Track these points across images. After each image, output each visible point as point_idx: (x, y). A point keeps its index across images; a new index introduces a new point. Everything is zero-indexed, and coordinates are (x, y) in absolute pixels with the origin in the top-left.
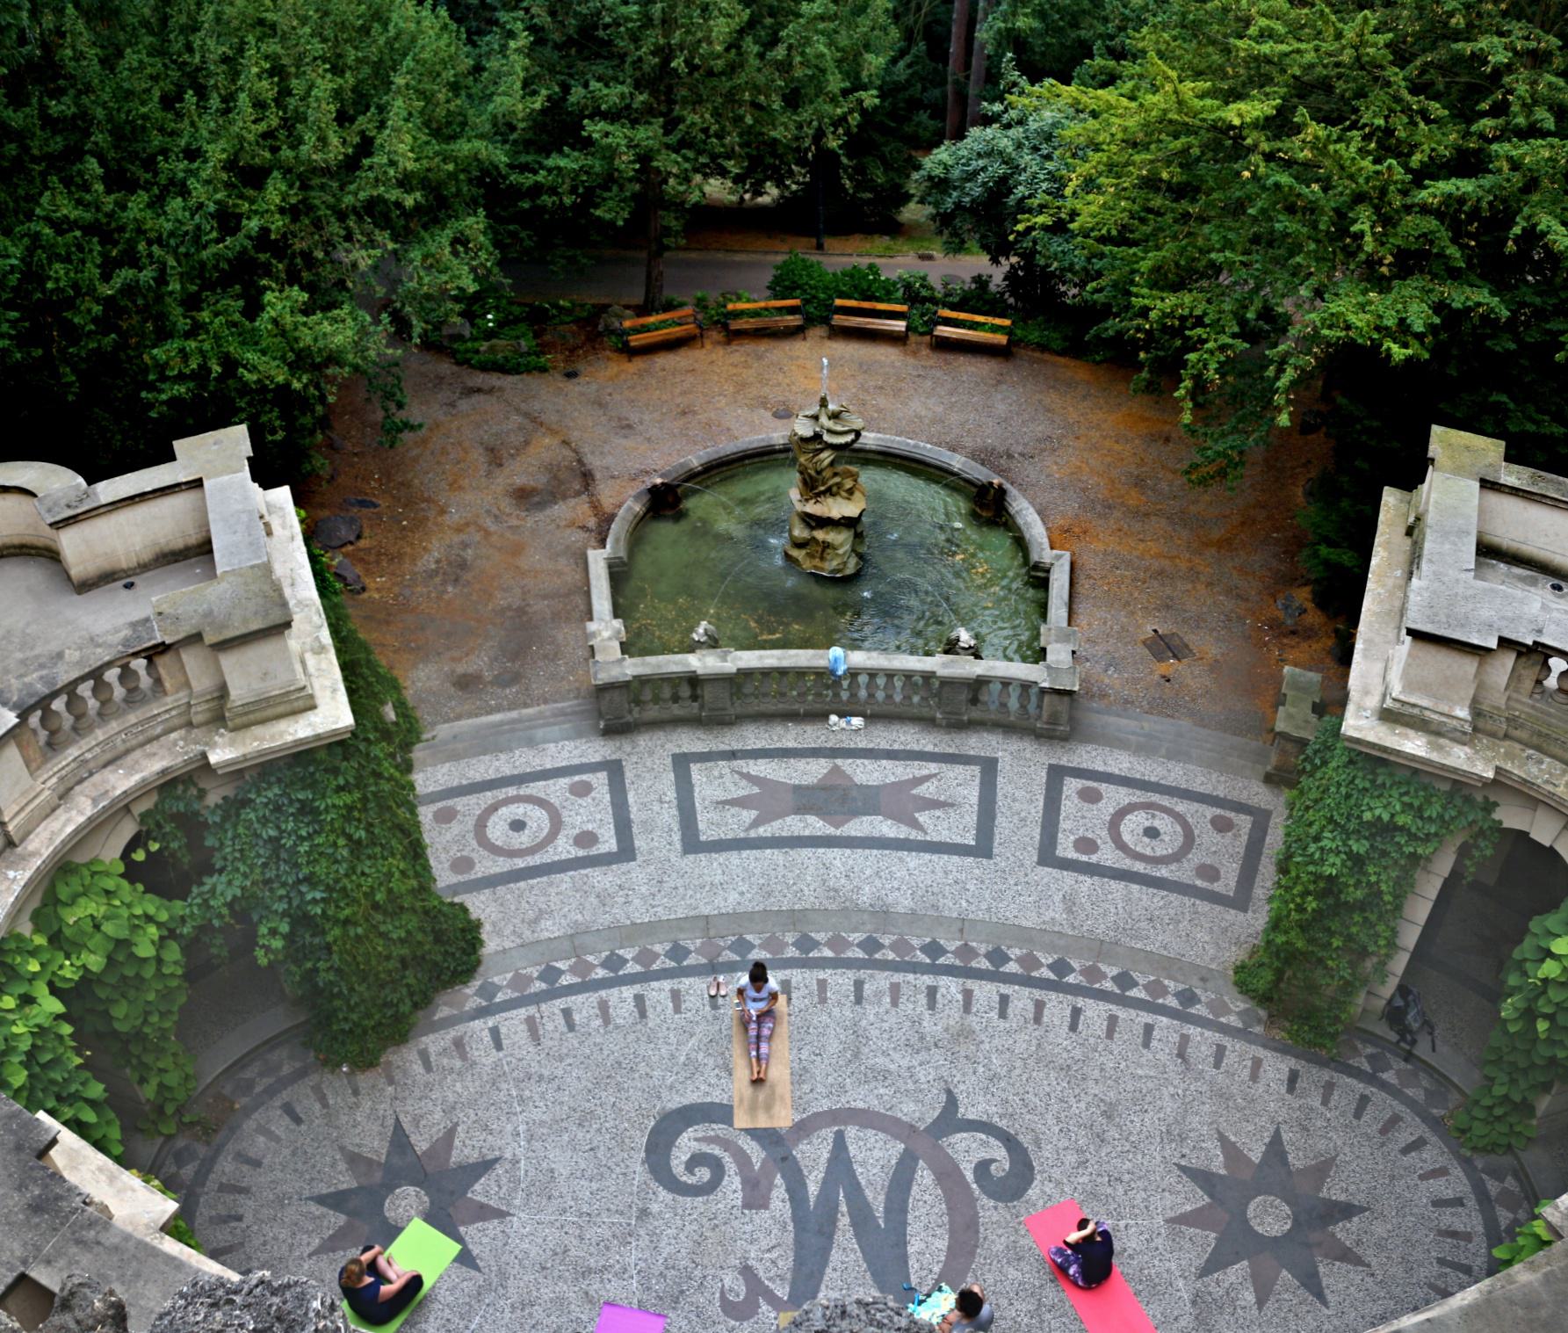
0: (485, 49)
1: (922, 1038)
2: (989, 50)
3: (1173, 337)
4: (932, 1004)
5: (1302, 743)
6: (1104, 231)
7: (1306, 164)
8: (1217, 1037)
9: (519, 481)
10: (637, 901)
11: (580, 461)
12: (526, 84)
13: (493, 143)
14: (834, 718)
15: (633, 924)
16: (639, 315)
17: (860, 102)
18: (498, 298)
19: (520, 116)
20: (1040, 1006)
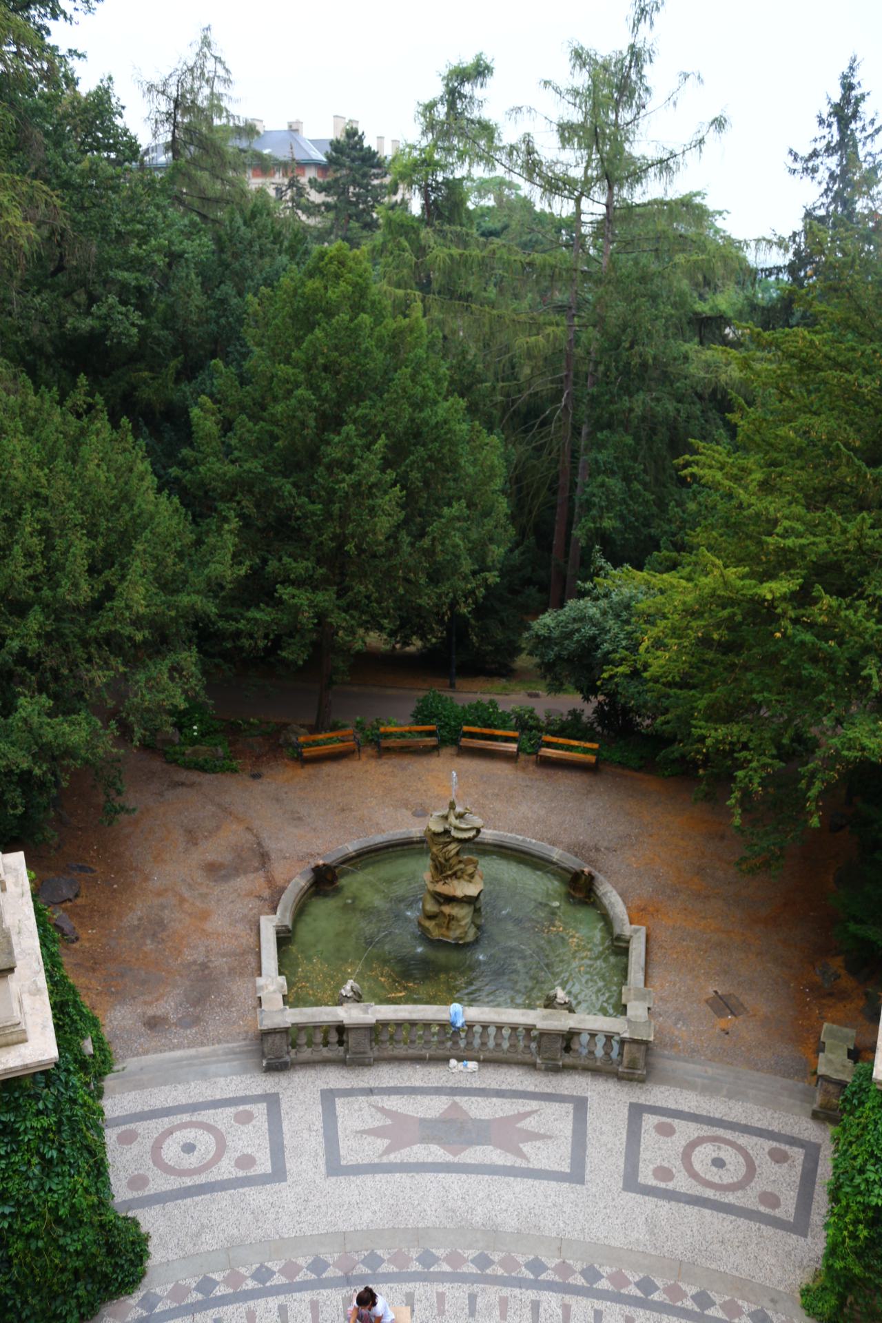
0: (205, 528)
2: (583, 543)
5: (842, 1085)
7: (824, 626)
9: (210, 857)
10: (285, 1218)
11: (259, 844)
12: (234, 556)
13: (207, 597)
14: (453, 1062)
15: (281, 1238)
16: (311, 733)
17: (486, 580)
19: (229, 579)
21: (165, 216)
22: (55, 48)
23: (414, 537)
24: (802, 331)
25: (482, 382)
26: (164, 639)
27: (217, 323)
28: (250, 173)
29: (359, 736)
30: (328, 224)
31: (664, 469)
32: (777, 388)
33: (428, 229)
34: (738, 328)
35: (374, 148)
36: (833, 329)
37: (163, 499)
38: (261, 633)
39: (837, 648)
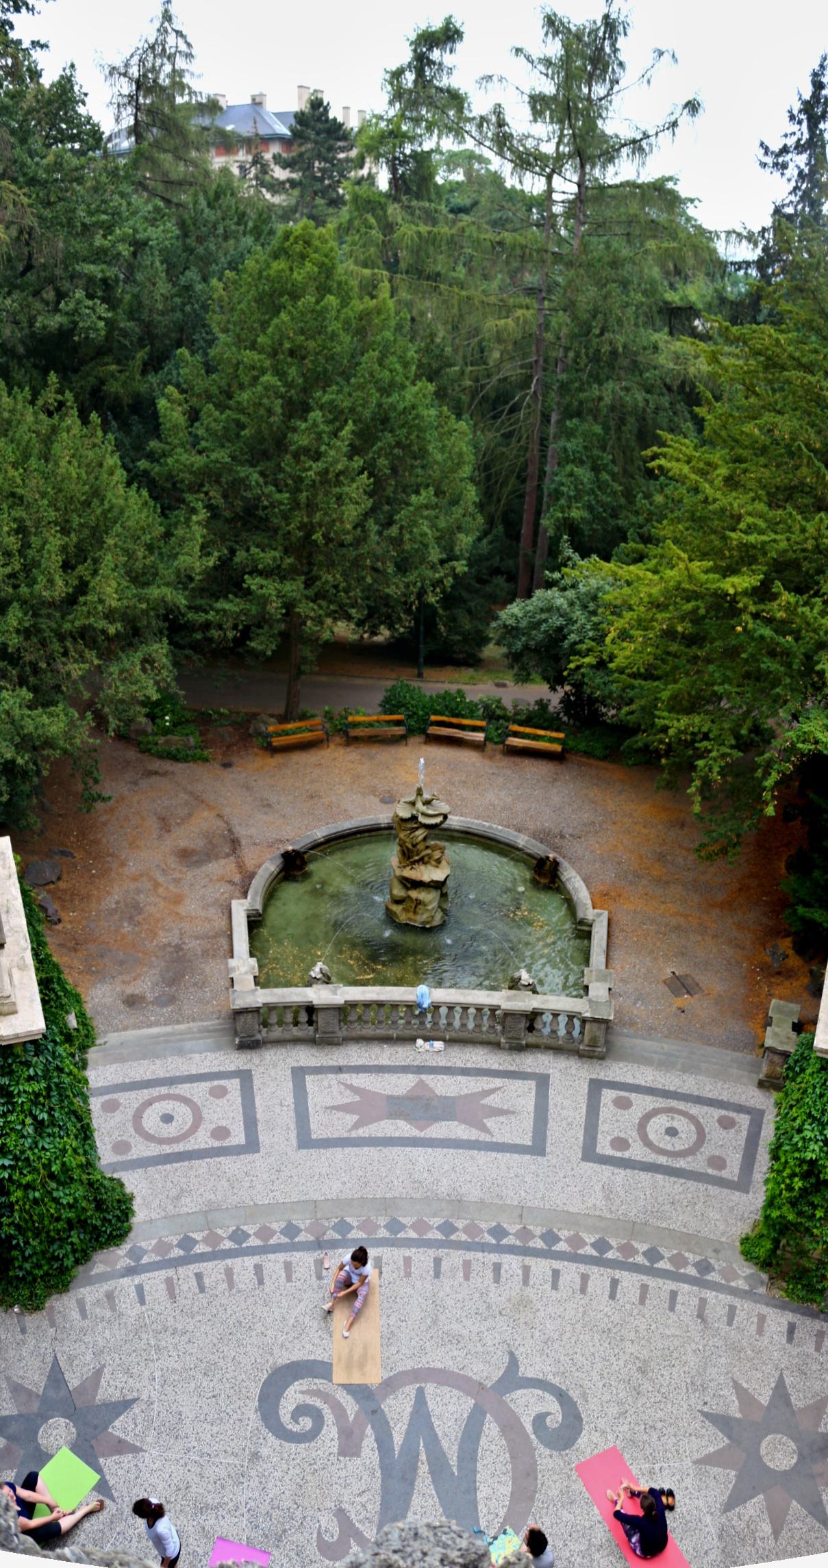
0: (174, 520)
1: (489, 1307)
3: (687, 747)
4: (497, 1279)
5: (786, 1055)
6: (635, 669)
7: (783, 622)
8: (729, 1299)
9: (183, 844)
11: (230, 831)
12: (203, 547)
13: (176, 589)
14: (420, 1042)
15: (256, 1205)
16: (280, 723)
17: (454, 569)
18: (174, 704)
19: (198, 571)
20: (585, 1278)
21: (129, 204)
22: (19, 42)
23: (381, 525)
24: (769, 329)
25: (451, 365)
26: (136, 632)
27: (182, 310)
28: (213, 151)
29: (328, 725)
30: (293, 202)
31: (632, 461)
32: (744, 384)
33: (396, 205)
34: (707, 321)
35: (340, 119)
36: (798, 330)
37: (132, 492)
38: (230, 624)
39: (793, 643)
